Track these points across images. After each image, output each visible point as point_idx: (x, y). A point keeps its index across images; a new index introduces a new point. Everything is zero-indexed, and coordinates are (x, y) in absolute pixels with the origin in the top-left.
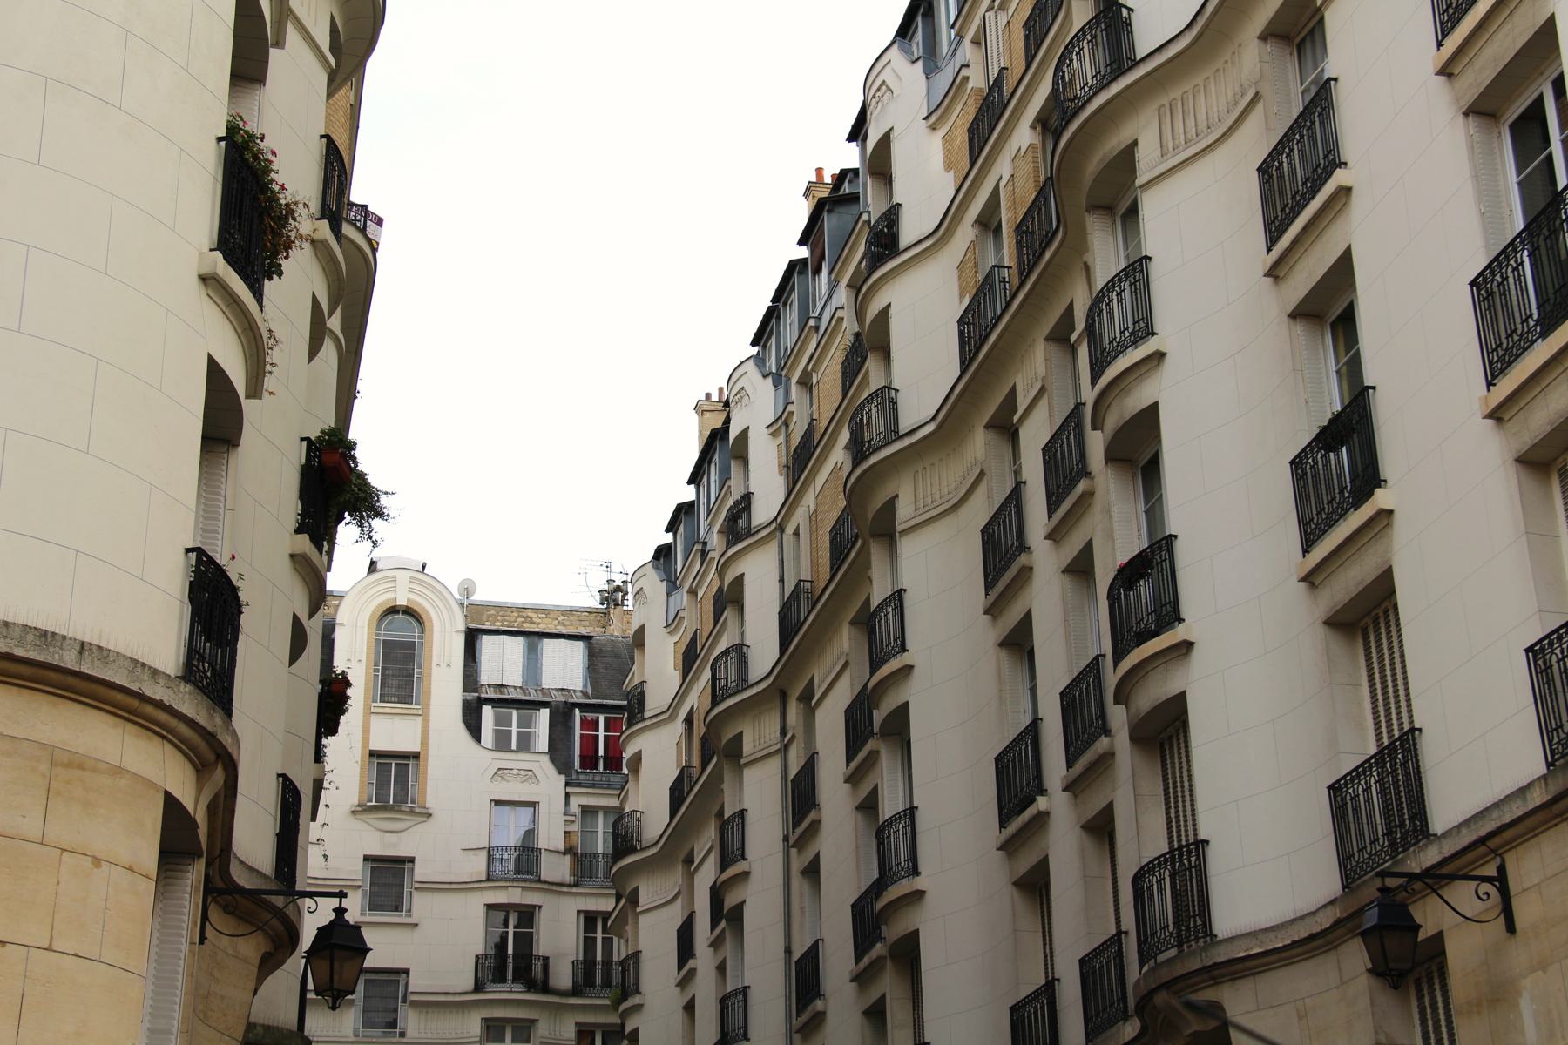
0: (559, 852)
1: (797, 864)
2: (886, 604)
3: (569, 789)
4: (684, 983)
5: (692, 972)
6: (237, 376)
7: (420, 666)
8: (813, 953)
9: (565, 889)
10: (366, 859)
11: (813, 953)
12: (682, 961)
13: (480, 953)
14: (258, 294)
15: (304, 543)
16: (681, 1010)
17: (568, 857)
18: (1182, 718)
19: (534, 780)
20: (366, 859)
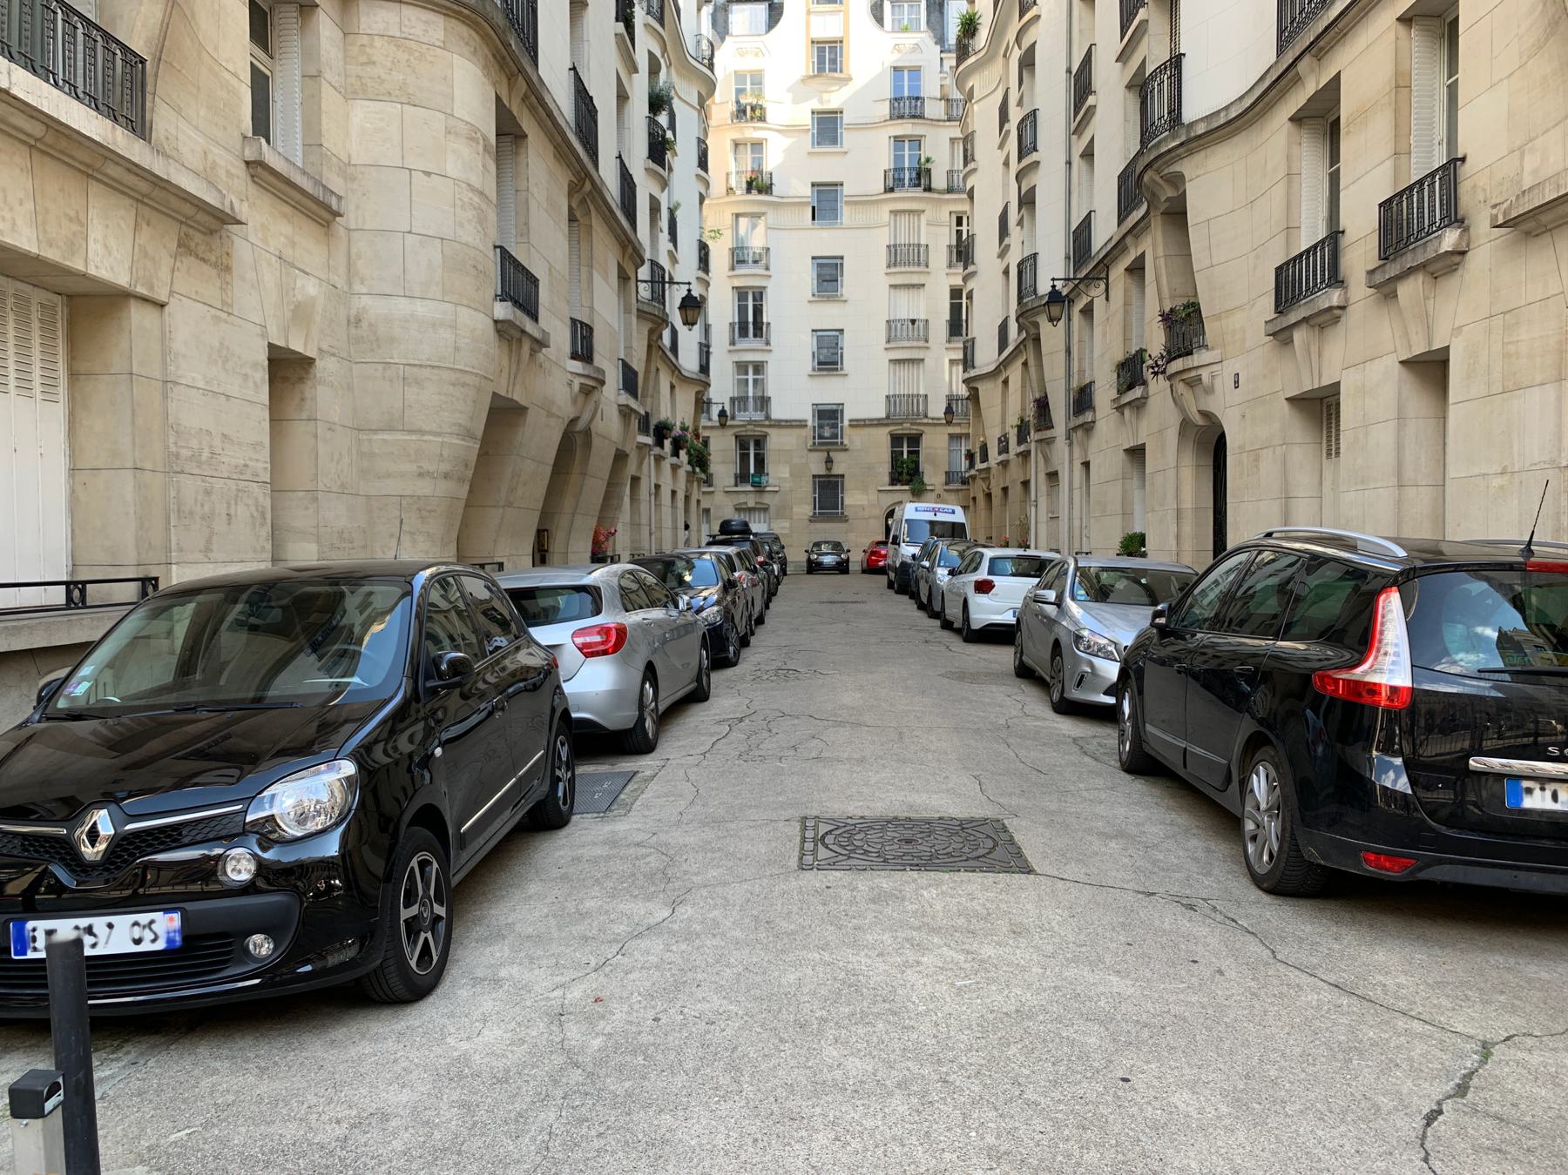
0: (936, 99)
1: (1079, 146)
2: (1161, 71)
3: (943, 55)
4: (1002, 255)
5: (1008, 246)
6: (658, 53)
7: (841, 56)
8: (1086, 223)
9: (941, 123)
10: (813, 185)
11: (1086, 223)
12: (1001, 240)
13: (887, 168)
14: (630, 79)
15: (701, 274)
16: (1002, 165)
17: (943, 102)
18: (1493, 711)
19: (919, 50)
20: (813, 185)
